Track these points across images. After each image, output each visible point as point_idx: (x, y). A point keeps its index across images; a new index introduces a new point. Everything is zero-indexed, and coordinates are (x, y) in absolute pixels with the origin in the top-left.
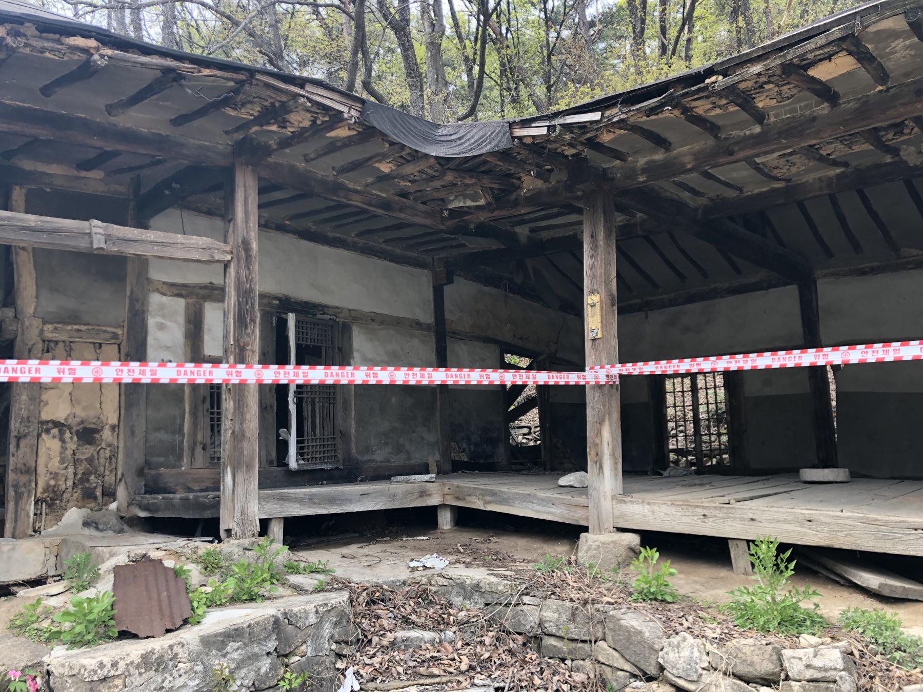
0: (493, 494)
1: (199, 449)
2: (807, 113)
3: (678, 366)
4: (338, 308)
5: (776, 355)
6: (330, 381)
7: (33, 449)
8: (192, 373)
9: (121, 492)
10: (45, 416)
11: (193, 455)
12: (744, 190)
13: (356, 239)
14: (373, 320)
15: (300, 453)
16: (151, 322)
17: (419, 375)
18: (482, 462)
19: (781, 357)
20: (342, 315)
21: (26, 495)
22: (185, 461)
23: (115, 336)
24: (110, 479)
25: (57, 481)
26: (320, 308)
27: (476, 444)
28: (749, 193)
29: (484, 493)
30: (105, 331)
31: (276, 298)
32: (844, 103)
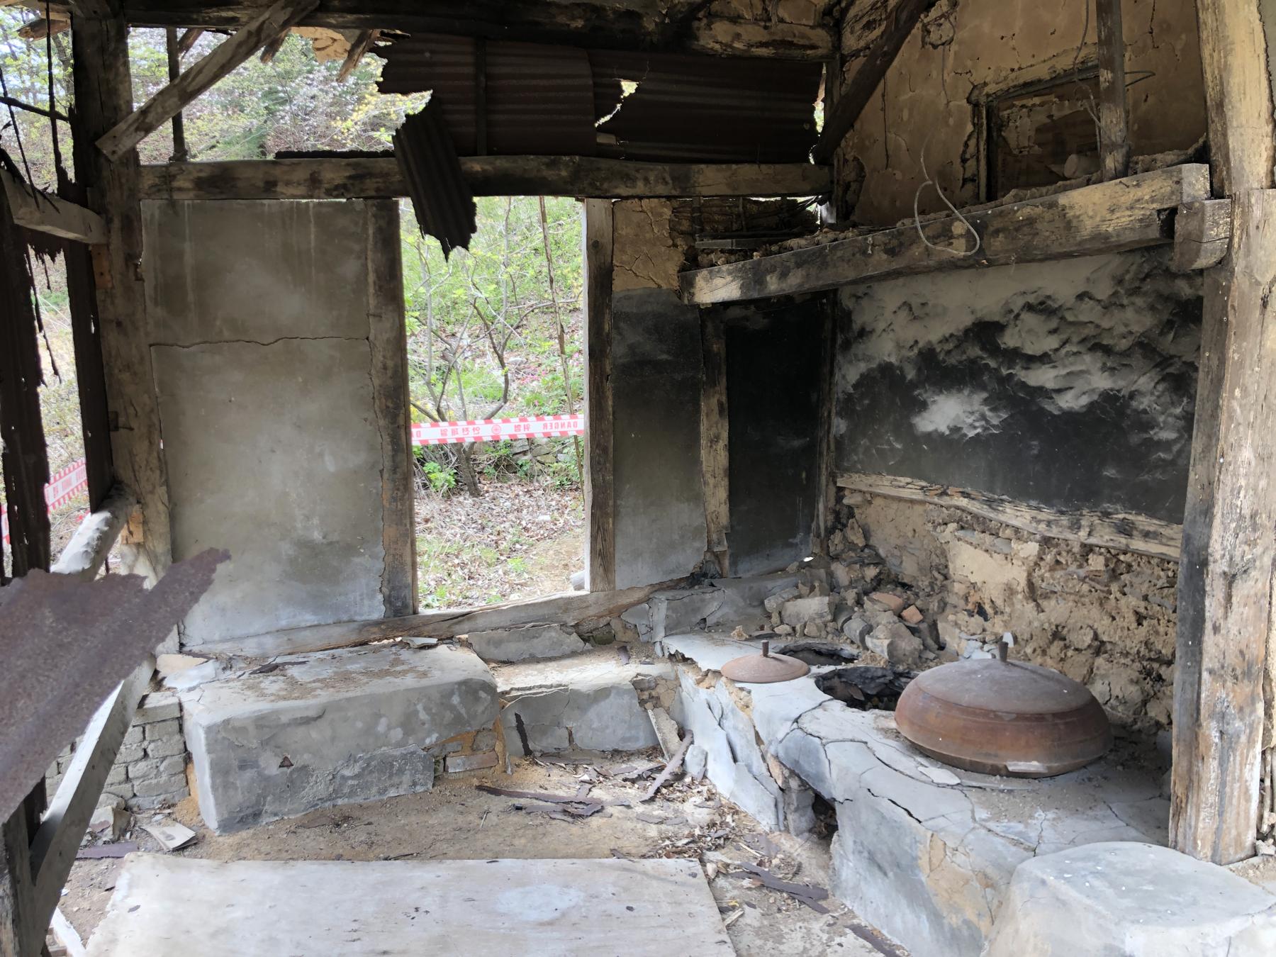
21: (1243, 739)
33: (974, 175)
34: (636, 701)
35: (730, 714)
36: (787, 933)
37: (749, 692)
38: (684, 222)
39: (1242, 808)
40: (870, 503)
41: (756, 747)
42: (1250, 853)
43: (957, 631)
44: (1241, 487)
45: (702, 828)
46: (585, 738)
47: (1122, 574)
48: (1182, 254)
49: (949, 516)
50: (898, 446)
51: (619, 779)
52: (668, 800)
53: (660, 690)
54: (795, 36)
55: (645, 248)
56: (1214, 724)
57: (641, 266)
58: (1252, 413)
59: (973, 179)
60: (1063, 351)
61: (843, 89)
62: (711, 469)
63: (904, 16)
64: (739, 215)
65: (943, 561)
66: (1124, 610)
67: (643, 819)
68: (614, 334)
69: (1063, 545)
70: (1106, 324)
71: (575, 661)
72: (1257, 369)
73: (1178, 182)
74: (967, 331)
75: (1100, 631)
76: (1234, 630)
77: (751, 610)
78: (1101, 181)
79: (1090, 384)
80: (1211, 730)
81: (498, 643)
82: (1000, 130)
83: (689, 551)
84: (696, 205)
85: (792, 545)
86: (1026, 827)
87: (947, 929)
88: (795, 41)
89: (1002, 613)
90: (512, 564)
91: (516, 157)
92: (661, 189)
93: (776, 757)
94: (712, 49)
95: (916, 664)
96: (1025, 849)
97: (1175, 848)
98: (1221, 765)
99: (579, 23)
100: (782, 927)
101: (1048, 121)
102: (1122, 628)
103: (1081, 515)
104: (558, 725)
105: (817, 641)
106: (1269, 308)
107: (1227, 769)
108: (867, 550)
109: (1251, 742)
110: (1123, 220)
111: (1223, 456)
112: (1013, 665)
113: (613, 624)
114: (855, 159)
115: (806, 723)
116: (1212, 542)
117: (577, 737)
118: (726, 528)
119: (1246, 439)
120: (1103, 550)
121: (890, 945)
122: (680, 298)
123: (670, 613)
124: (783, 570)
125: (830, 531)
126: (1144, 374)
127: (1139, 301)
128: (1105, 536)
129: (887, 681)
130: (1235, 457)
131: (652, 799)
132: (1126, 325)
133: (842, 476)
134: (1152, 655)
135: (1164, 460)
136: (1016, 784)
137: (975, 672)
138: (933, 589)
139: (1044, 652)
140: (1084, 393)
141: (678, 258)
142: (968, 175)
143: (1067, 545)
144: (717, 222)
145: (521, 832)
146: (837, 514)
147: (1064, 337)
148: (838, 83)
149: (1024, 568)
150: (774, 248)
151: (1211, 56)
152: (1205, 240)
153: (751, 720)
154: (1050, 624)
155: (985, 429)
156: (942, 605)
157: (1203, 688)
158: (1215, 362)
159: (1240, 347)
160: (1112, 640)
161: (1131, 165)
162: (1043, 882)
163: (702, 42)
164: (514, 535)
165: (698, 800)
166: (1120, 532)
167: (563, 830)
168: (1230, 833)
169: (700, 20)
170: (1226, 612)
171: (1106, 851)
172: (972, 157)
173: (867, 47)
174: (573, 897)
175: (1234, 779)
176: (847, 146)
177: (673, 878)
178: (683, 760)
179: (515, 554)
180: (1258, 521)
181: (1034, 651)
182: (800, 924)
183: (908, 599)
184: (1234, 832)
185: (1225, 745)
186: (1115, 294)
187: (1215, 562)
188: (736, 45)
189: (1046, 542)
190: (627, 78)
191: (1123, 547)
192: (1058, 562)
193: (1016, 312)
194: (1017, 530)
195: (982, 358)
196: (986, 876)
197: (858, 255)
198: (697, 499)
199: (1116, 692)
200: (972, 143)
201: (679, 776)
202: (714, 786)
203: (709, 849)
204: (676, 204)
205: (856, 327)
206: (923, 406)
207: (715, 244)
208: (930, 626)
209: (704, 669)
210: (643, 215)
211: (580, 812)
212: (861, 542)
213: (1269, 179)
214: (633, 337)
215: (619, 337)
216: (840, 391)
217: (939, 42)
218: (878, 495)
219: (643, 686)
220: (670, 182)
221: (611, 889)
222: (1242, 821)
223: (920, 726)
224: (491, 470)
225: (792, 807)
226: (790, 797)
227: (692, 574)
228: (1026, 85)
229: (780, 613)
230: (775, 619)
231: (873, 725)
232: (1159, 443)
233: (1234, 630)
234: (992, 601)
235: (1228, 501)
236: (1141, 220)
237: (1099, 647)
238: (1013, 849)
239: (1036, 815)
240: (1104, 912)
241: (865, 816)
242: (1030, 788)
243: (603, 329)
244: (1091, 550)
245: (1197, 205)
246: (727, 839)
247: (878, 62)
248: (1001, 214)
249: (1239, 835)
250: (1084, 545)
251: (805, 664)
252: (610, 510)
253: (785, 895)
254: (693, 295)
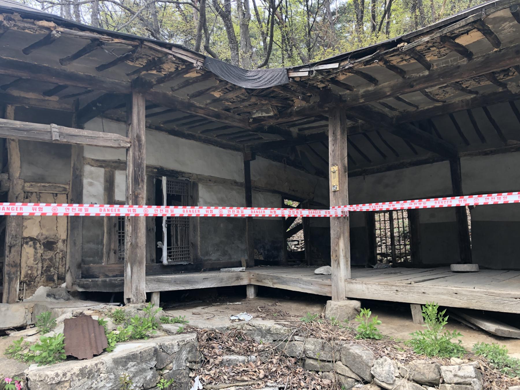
0: (278, 278)
1: (112, 253)
2: (455, 64)
3: (382, 206)
4: (190, 173)
5: (437, 200)
6: (186, 215)
7: (18, 253)
8: (108, 210)
9: (68, 277)
10: (25, 235)
11: (108, 256)
12: (419, 107)
13: (201, 135)
14: (210, 180)
15: (169, 255)
16: (85, 181)
17: (236, 211)
18: (271, 260)
19: (440, 201)
20: (193, 178)
21: (14, 279)
22: (104, 260)
23: (65, 190)
24: (62, 270)
25: (32, 271)
26: (180, 174)
27: (268, 250)
28: (422, 109)
29: (273, 278)
30: (59, 187)
31: (156, 168)
32: (476, 58)
76: (12, 257)
233: (12, 257)
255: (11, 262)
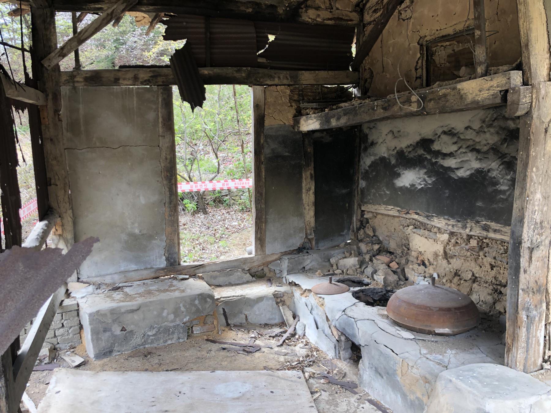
21: (537, 319)
33: (421, 76)
34: (275, 303)
35: (315, 308)
36: (340, 403)
37: (324, 299)
38: (295, 96)
39: (536, 349)
40: (376, 217)
41: (326, 322)
42: (540, 368)
43: (413, 272)
44: (536, 210)
45: (303, 357)
46: (252, 318)
47: (484, 248)
48: (510, 110)
49: (410, 223)
50: (388, 193)
51: (267, 336)
52: (288, 345)
53: (285, 298)
54: (343, 15)
55: (278, 107)
56: (524, 312)
57: (277, 115)
58: (541, 178)
59: (420, 77)
60: (459, 152)
61: (364, 38)
62: (307, 202)
63: (390, 7)
64: (319, 93)
65: (407, 242)
66: (485, 263)
67: (278, 353)
68: (265, 144)
69: (459, 235)
70: (477, 140)
71: (248, 285)
72: (543, 159)
73: (509, 79)
74: (418, 143)
75: (475, 272)
76: (533, 272)
77: (324, 263)
78: (475, 78)
79: (470, 166)
80: (523, 315)
81: (215, 278)
82: (432, 56)
83: (298, 238)
84: (300, 88)
85: (342, 235)
86: (443, 357)
87: (409, 401)
88: (343, 18)
89: (433, 264)
90: (221, 243)
91: (223, 68)
92: (285, 82)
93: (335, 327)
94: (307, 21)
95: (395, 287)
96: (442, 366)
97: (507, 366)
98: (527, 330)
99: (250, 10)
100: (338, 400)
101: (452, 52)
102: (485, 271)
103: (467, 222)
104: (241, 313)
105: (353, 277)
106: (548, 133)
107: (530, 332)
108: (374, 238)
109: (540, 320)
110: (485, 95)
111: (528, 197)
112: (437, 287)
113: (265, 269)
114: (369, 69)
115: (348, 312)
116: (523, 234)
117: (249, 318)
118: (314, 228)
119: (538, 189)
120: (476, 237)
121: (384, 408)
122: (294, 128)
123: (289, 265)
124: (338, 246)
125: (358, 229)
126: (494, 161)
127: (492, 130)
128: (477, 231)
129: (383, 294)
130: (533, 197)
131: (282, 345)
132: (486, 140)
133: (364, 206)
134: (498, 283)
135: (502, 199)
136: (439, 339)
137: (421, 290)
138: (403, 254)
139: (451, 282)
140: (468, 170)
141: (293, 111)
142: (418, 75)
143: (461, 235)
144: (310, 96)
145: (225, 359)
146: (361, 222)
147: (460, 145)
148: (362, 36)
149: (442, 245)
150: (334, 107)
151: (523, 24)
152: (520, 104)
153: (324, 311)
154: (454, 269)
155: (425, 185)
156: (407, 261)
157: (520, 297)
158: (525, 156)
159: (535, 150)
160: (480, 276)
161: (488, 71)
162: (451, 381)
163: (303, 18)
164: (222, 231)
165: (302, 345)
166: (484, 230)
167: (243, 358)
168: (531, 359)
169: (302, 8)
170: (530, 264)
171: (477, 367)
172: (420, 68)
173: (375, 20)
174: (248, 387)
175: (533, 336)
176: (366, 63)
177: (291, 379)
178: (295, 328)
179: (222, 239)
180: (543, 225)
181: (447, 281)
182: (345, 399)
183: (392, 258)
184: (533, 359)
185: (529, 321)
186: (482, 127)
187: (525, 242)
188: (318, 19)
189: (452, 234)
190: (271, 34)
191: (485, 236)
192: (457, 243)
193: (439, 134)
194: (439, 229)
195: (424, 155)
196: (426, 378)
197: (370, 110)
198: (301, 215)
199: (482, 298)
200: (420, 62)
201: (293, 335)
202: (308, 339)
203: (306, 367)
204: (292, 88)
205: (370, 141)
206: (399, 175)
207: (309, 105)
208: (401, 270)
209: (304, 289)
210: (278, 93)
211: (251, 350)
212: (372, 234)
213: (548, 77)
214: (273, 145)
215: (267, 146)
216: (363, 169)
217: (406, 18)
218: (379, 214)
219: (277, 296)
220: (289, 78)
221: (264, 384)
222: (536, 354)
223: (397, 313)
224: (212, 203)
225: (342, 348)
226: (341, 344)
227: (299, 248)
228: (443, 37)
229: (337, 265)
230: (335, 267)
231: (377, 313)
232: (501, 191)
233: (533, 272)
234: (428, 259)
235: (530, 216)
236: (493, 95)
237: (475, 279)
238: (438, 366)
239: (447, 352)
240: (477, 394)
241: (374, 352)
242: (445, 340)
243: (260, 142)
244: (471, 238)
245: (517, 88)
246: (314, 362)
247: (379, 27)
248: (432, 92)
249: (535, 360)
250: (468, 235)
251: (348, 287)
252: (263, 220)
253: (339, 386)
254: (299, 127)
255: (532, 284)
